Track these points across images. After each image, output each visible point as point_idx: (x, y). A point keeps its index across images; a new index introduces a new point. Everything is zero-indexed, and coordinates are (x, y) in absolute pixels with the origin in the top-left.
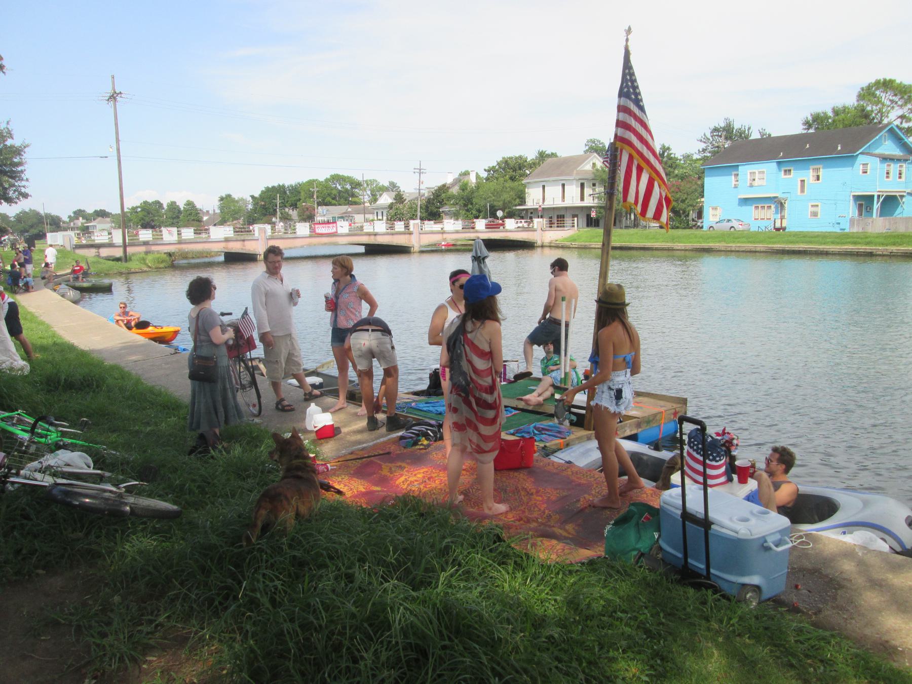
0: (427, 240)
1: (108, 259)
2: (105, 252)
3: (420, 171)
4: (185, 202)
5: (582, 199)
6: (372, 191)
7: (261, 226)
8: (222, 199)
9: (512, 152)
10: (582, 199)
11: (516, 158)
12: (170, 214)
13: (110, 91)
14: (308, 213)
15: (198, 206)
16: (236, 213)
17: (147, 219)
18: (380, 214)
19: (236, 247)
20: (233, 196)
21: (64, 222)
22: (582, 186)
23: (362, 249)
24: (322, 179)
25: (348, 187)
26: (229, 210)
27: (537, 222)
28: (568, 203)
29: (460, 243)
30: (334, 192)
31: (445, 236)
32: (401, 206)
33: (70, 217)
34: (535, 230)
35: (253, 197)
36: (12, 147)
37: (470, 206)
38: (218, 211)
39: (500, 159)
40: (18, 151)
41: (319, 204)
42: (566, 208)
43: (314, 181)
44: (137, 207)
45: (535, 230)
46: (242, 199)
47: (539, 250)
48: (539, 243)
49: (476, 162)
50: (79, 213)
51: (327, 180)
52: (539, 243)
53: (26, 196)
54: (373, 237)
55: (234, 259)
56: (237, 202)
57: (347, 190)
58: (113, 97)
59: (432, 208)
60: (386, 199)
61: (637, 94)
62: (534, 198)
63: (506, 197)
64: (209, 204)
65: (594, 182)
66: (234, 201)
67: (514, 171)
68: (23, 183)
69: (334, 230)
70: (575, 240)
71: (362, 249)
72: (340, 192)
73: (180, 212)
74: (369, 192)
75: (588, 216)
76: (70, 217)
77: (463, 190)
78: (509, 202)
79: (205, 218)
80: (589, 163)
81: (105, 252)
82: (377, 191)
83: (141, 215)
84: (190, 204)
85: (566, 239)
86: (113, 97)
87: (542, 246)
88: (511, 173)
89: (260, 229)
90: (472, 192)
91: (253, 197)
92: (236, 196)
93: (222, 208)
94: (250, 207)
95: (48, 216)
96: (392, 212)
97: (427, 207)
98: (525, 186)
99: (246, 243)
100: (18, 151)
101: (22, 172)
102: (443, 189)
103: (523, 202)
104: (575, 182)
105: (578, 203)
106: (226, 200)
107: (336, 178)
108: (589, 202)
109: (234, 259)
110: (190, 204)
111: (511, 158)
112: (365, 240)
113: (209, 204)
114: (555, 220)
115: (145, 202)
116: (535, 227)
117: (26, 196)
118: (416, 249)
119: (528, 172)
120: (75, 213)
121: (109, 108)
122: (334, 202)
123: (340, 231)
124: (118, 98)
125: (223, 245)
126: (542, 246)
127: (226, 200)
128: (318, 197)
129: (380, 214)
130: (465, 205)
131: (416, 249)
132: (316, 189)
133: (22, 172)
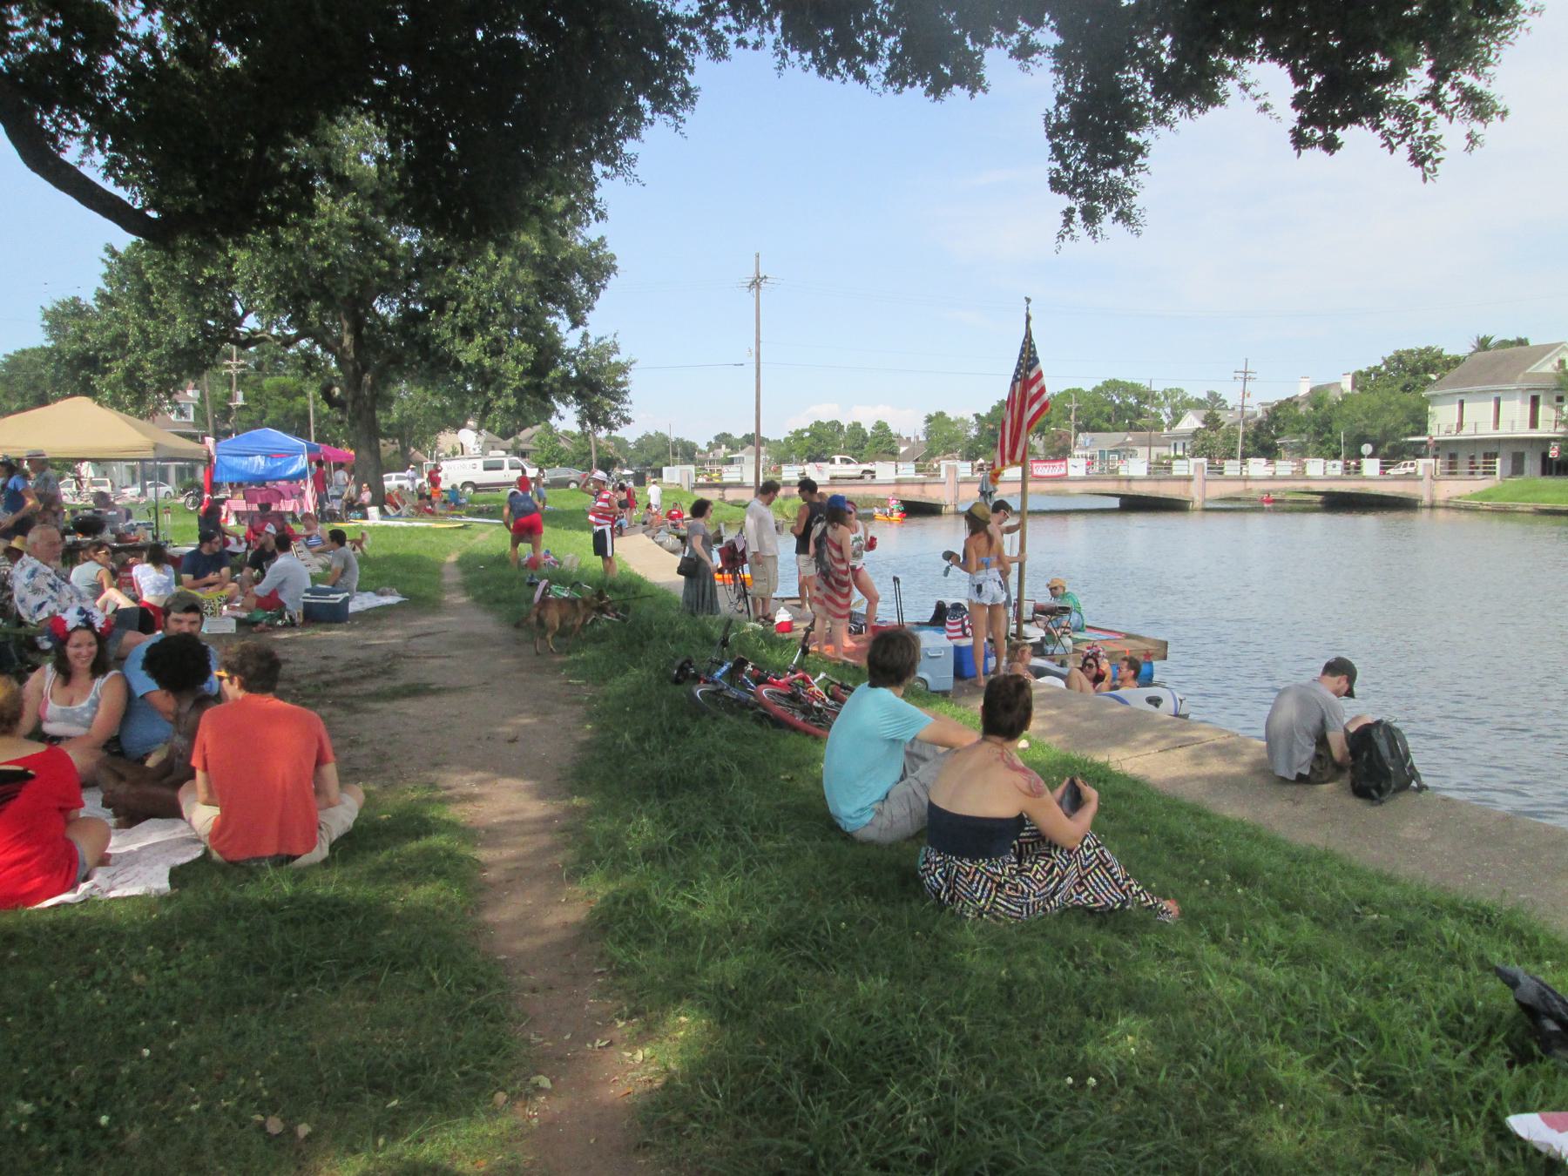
0: (1218, 489)
1: (733, 504)
2: (731, 495)
3: (1246, 376)
4: (873, 423)
5: (1534, 423)
6: (1174, 408)
7: (951, 463)
8: (929, 419)
9: (1414, 342)
10: (1534, 423)
11: (1421, 352)
12: (850, 442)
13: (753, 275)
14: (1060, 443)
15: (894, 431)
16: (950, 442)
17: (816, 450)
18: (1180, 447)
19: (913, 494)
20: (948, 415)
21: (701, 452)
22: (1535, 401)
23: (1116, 503)
24: (1088, 387)
25: (1132, 401)
26: (942, 437)
27: (1422, 465)
28: (1504, 432)
29: (1289, 498)
30: (1107, 409)
31: (1250, 485)
32: (1213, 434)
33: (709, 444)
34: (1420, 479)
35: (977, 416)
36: (618, 363)
37: (1327, 435)
38: (923, 438)
39: (1389, 353)
40: (622, 369)
41: (1079, 429)
42: (1499, 441)
43: (1074, 391)
44: (804, 431)
45: (1420, 479)
46: (962, 420)
47: (1426, 512)
48: (1426, 500)
49: (1327, 363)
50: (723, 439)
51: (1097, 390)
52: (1426, 500)
53: (628, 421)
54: (1124, 484)
55: (916, 510)
56: (954, 424)
57: (1130, 407)
58: (756, 283)
59: (1264, 439)
60: (1191, 422)
61: (1023, 350)
62: (1442, 421)
63: (1388, 420)
64: (909, 425)
65: (1560, 393)
66: (948, 422)
67: (1417, 372)
68: (626, 406)
69: (1063, 471)
70: (1489, 498)
71: (1116, 503)
72: (1118, 407)
73: (865, 439)
74: (1168, 410)
75: (1545, 456)
76: (709, 444)
77: (1316, 408)
78: (1396, 429)
79: (902, 449)
80: (1550, 360)
81: (731, 495)
82: (1182, 406)
83: (807, 443)
84: (881, 427)
85: (1475, 496)
86: (756, 283)
87: (1432, 507)
88: (1408, 377)
89: (948, 467)
90: (1332, 409)
91: (977, 416)
92: (951, 415)
93: (928, 433)
94: (973, 432)
95: (680, 442)
96: (1198, 443)
97: (1256, 436)
98: (1427, 401)
99: (927, 488)
100: (622, 369)
101: (625, 392)
102: (1291, 403)
103: (1422, 428)
104: (1519, 394)
105: (1524, 432)
106: (936, 422)
107: (1112, 386)
108: (1545, 430)
109: (916, 510)
110: (881, 427)
111: (1410, 352)
112: (1124, 488)
113: (909, 425)
114: (1480, 461)
115: (818, 423)
116: (1420, 473)
117: (628, 421)
118: (1198, 504)
119: (1433, 377)
120: (717, 438)
121: (750, 297)
122: (1105, 425)
123: (1072, 473)
124: (763, 285)
125: (893, 489)
126: (1432, 507)
127: (936, 422)
128: (1077, 418)
129: (1180, 447)
130: (1319, 434)
131: (1198, 504)
132: (1075, 405)
133: (625, 392)
